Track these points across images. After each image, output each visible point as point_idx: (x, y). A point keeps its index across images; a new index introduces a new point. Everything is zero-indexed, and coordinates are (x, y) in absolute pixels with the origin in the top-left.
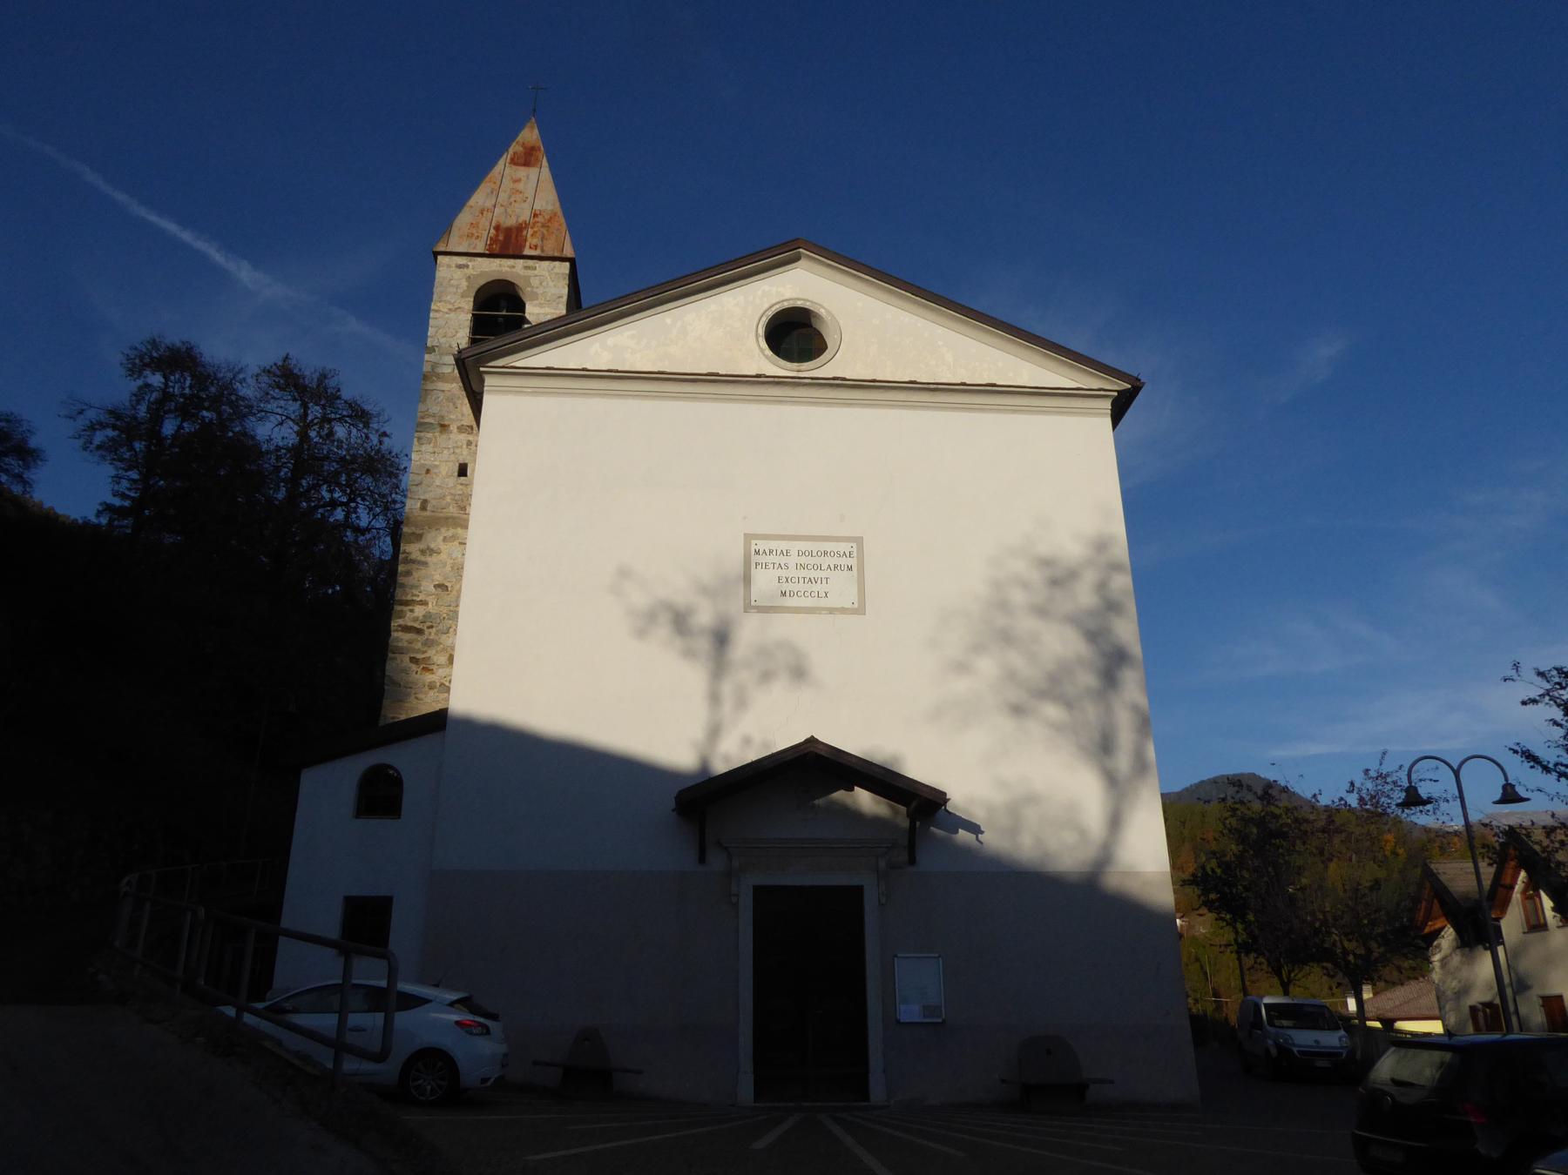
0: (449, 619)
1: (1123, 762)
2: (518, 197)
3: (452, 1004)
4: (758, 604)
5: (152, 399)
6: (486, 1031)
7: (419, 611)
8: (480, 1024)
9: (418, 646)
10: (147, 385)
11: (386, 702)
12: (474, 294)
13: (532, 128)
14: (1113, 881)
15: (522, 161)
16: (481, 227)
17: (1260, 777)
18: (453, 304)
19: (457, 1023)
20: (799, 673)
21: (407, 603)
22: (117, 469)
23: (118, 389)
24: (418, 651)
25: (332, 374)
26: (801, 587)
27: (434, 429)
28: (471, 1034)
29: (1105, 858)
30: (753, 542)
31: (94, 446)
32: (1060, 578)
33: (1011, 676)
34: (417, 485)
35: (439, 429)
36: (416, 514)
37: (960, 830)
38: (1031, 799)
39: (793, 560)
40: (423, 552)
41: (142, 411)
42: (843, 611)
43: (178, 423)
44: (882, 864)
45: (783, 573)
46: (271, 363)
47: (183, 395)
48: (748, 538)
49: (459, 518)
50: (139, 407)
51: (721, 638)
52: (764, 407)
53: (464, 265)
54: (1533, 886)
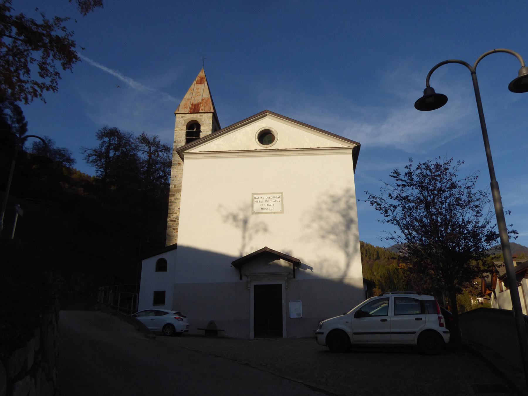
1: (351, 249)
2: (198, 94)
3: (174, 314)
4: (255, 212)
5: (106, 145)
6: (182, 320)
7: (175, 216)
8: (182, 319)
9: (175, 225)
10: (104, 142)
11: (167, 241)
13: (202, 71)
14: (347, 281)
15: (199, 82)
16: (188, 104)
17: (517, 244)
18: (180, 128)
19: (175, 318)
20: (265, 230)
21: (171, 214)
22: (97, 168)
23: (96, 144)
24: (175, 227)
25: (157, 137)
26: (267, 207)
28: (178, 320)
29: (345, 274)
30: (254, 195)
31: (90, 161)
32: (335, 200)
33: (321, 228)
34: (173, 181)
35: (178, 164)
36: (173, 189)
37: (307, 269)
38: (326, 260)
39: (264, 200)
40: (175, 199)
41: (103, 150)
43: (114, 152)
44: (286, 278)
45: (262, 203)
46: (139, 136)
47: (115, 144)
48: (253, 194)
50: (102, 149)
51: (245, 222)
52: (257, 158)
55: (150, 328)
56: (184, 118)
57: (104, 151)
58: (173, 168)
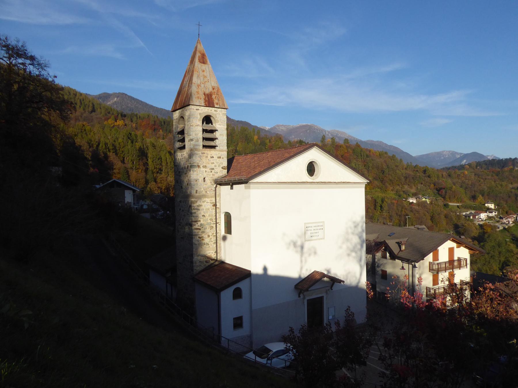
7: (199, 223)
12: (202, 120)
24: (200, 235)
26: (315, 234)
27: (196, 167)
34: (194, 185)
42: (321, 239)
51: (302, 247)
54: (385, 250)
55: (278, 367)
56: (199, 111)
57: (112, 147)
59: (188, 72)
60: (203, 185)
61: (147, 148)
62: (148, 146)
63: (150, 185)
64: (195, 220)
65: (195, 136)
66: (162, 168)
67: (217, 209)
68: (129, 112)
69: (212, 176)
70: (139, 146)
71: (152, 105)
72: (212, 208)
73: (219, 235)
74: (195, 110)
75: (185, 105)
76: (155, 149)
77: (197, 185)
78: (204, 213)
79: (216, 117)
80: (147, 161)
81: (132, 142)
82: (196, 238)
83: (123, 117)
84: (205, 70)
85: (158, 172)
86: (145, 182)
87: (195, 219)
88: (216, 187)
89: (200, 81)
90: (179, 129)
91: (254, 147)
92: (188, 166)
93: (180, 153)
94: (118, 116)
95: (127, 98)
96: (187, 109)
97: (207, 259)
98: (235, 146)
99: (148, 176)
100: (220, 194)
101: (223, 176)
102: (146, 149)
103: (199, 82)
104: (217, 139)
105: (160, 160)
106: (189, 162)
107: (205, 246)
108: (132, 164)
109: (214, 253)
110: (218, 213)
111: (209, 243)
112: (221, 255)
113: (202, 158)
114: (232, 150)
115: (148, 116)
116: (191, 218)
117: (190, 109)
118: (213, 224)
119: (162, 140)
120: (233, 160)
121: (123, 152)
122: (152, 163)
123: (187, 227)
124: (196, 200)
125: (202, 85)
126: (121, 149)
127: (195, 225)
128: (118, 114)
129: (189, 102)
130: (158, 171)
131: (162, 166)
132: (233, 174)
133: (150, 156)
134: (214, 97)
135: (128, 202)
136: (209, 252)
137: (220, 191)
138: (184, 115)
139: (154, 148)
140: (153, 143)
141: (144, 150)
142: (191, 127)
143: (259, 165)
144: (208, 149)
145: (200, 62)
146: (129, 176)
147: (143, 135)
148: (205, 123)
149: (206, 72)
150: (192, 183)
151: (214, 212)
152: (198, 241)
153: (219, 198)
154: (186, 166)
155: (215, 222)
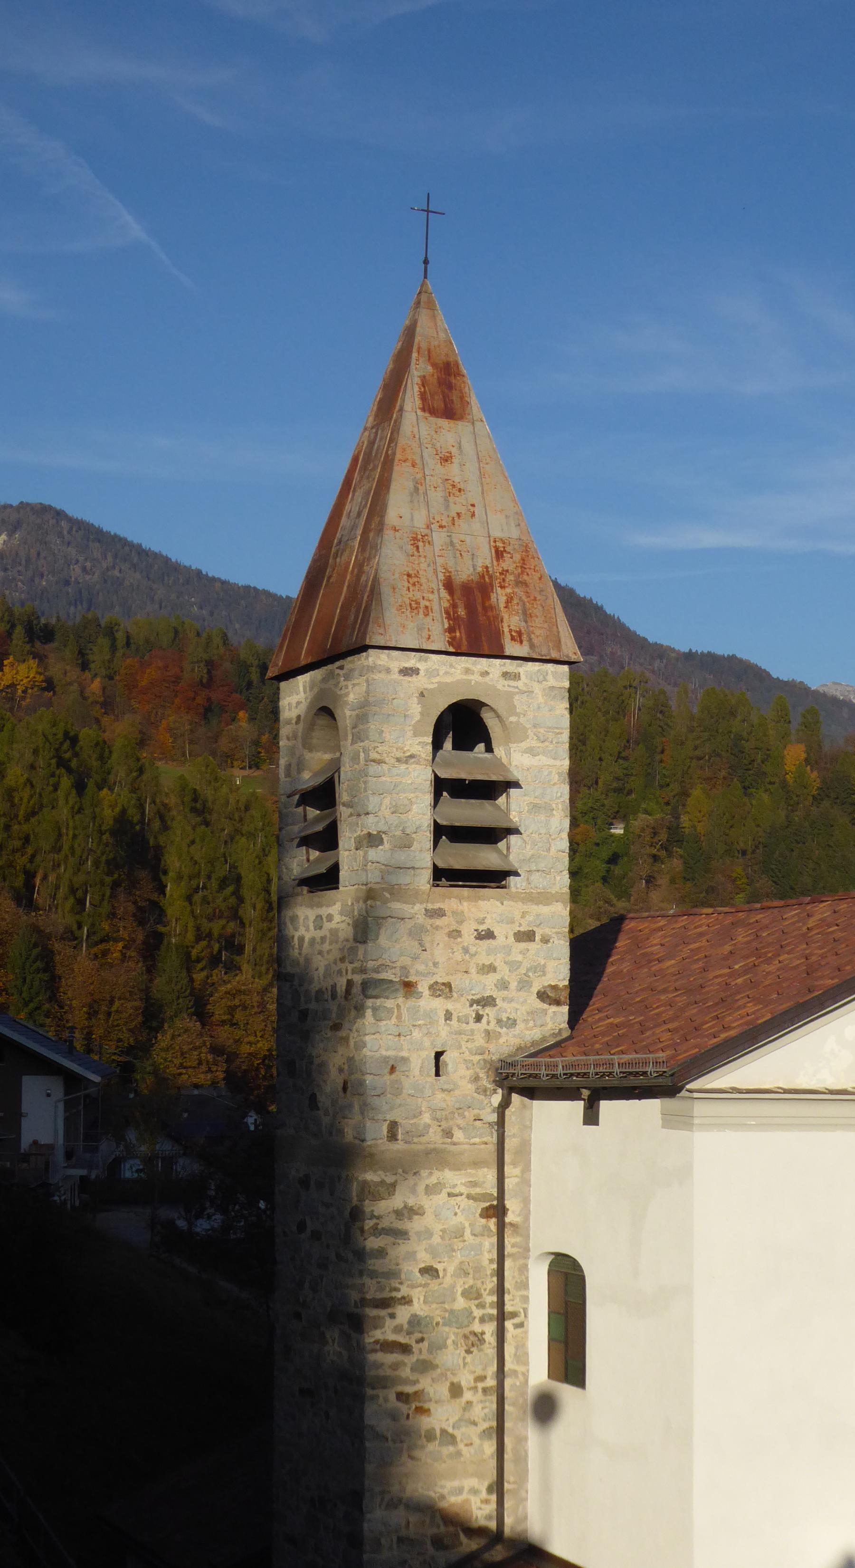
0: (445, 1325)
7: (403, 1314)
24: (407, 1382)
27: (397, 990)
35: (402, 991)
49: (443, 1151)
53: (411, 669)
56: (414, 679)
58: (375, 1009)
59: (364, 468)
60: (428, 1092)
61: (162, 818)
62: (165, 805)
63: (168, 1036)
64: (379, 1296)
65: (393, 819)
66: (242, 935)
67: (508, 1232)
68: (72, 610)
69: (480, 1041)
70: (118, 810)
71: (199, 572)
72: (478, 1230)
73: (513, 1386)
74: (396, 676)
75: (344, 650)
76: (203, 827)
77: (398, 1091)
78: (433, 1251)
79: (512, 710)
80: (155, 896)
81: (80, 787)
82: (386, 1400)
83: (38, 644)
84: (454, 451)
85: (215, 961)
86: (140, 1019)
87: (381, 1289)
88: (505, 1104)
89: (424, 512)
90: (306, 775)
91: (782, 813)
92: (350, 983)
93: (307, 907)
94: (9, 633)
95: (65, 533)
96: (352, 670)
97: (443, 1529)
98: (667, 804)
99: (160, 982)
100: (524, 1149)
101: (544, 1039)
102: (157, 824)
103: (420, 521)
104: (516, 831)
105: (231, 889)
106: (357, 964)
107: (432, 1447)
108: (72, 910)
109: (484, 1494)
110: (510, 1255)
111: (458, 1434)
112: (525, 1508)
113: (427, 939)
114: (648, 831)
115: (172, 635)
116: (358, 1281)
117: (372, 669)
118: (482, 1320)
119: (246, 772)
120: (615, 940)
121: (27, 840)
122: (186, 904)
123: (333, 1334)
124: (390, 1179)
125: (439, 538)
126: (16, 827)
127: (378, 1323)
128: (13, 626)
129: (364, 633)
130: (220, 952)
131: (242, 924)
132: (603, 1034)
133: (177, 864)
134: (502, 600)
135: (35, 1142)
136: (456, 1483)
137: (527, 1127)
138: (336, 698)
139: (199, 819)
140: (195, 790)
141: (143, 829)
142: (373, 769)
143: (752, 984)
144: (466, 891)
145: (429, 408)
146: (53, 984)
147: (142, 743)
148: (448, 745)
149: (462, 465)
150: (369, 1079)
151: (490, 1252)
152: (394, 1416)
153: (517, 1171)
154: (342, 983)
155: (494, 1312)
